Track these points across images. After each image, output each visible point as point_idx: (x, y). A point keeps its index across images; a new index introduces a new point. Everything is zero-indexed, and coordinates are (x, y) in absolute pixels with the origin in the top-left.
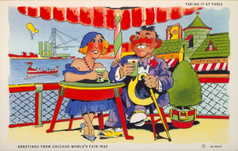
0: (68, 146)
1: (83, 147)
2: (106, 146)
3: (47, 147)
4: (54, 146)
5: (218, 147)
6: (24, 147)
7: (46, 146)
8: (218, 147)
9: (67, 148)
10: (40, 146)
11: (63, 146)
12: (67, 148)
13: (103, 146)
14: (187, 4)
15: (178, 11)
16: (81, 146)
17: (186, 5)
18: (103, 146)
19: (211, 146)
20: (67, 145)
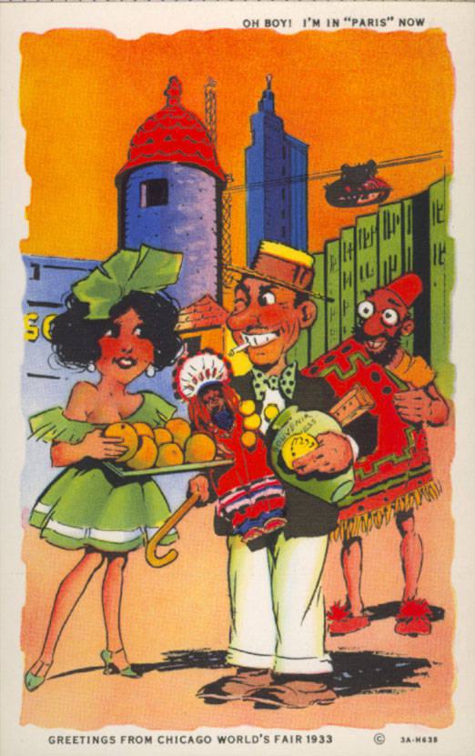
0: (208, 740)
1: (255, 739)
2: (326, 739)
4: (161, 740)
7: (206, 737)
9: (204, 743)
13: (319, 739)
16: (249, 739)
19: (403, 738)
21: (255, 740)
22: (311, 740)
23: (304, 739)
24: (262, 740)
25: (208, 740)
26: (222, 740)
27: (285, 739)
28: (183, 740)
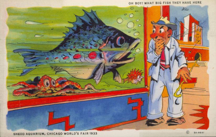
0: (130, 3)
2: (95, 133)
3: (138, 3)
4: (48, 134)
5: (201, 133)
6: (196, 3)
7: (61, 133)
8: (201, 133)
9: (30, 135)
10: (80, 133)
11: (57, 134)
12: (22, 135)
13: (93, 133)
14: (174, 3)
15: (136, 40)
17: (173, 4)
18: (93, 133)
19: (195, 132)
20: (60, 133)
21: (75, 134)
22: (52, 133)
23: (89, 134)
24: (77, 134)
25: (61, 134)
26: (65, 134)
27: (84, 134)
28: (54, 134)
